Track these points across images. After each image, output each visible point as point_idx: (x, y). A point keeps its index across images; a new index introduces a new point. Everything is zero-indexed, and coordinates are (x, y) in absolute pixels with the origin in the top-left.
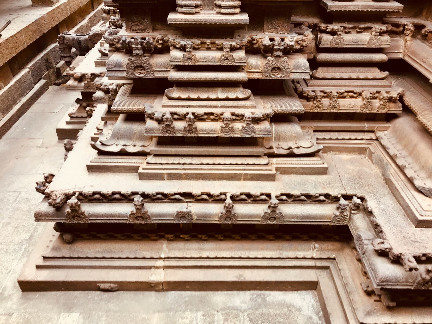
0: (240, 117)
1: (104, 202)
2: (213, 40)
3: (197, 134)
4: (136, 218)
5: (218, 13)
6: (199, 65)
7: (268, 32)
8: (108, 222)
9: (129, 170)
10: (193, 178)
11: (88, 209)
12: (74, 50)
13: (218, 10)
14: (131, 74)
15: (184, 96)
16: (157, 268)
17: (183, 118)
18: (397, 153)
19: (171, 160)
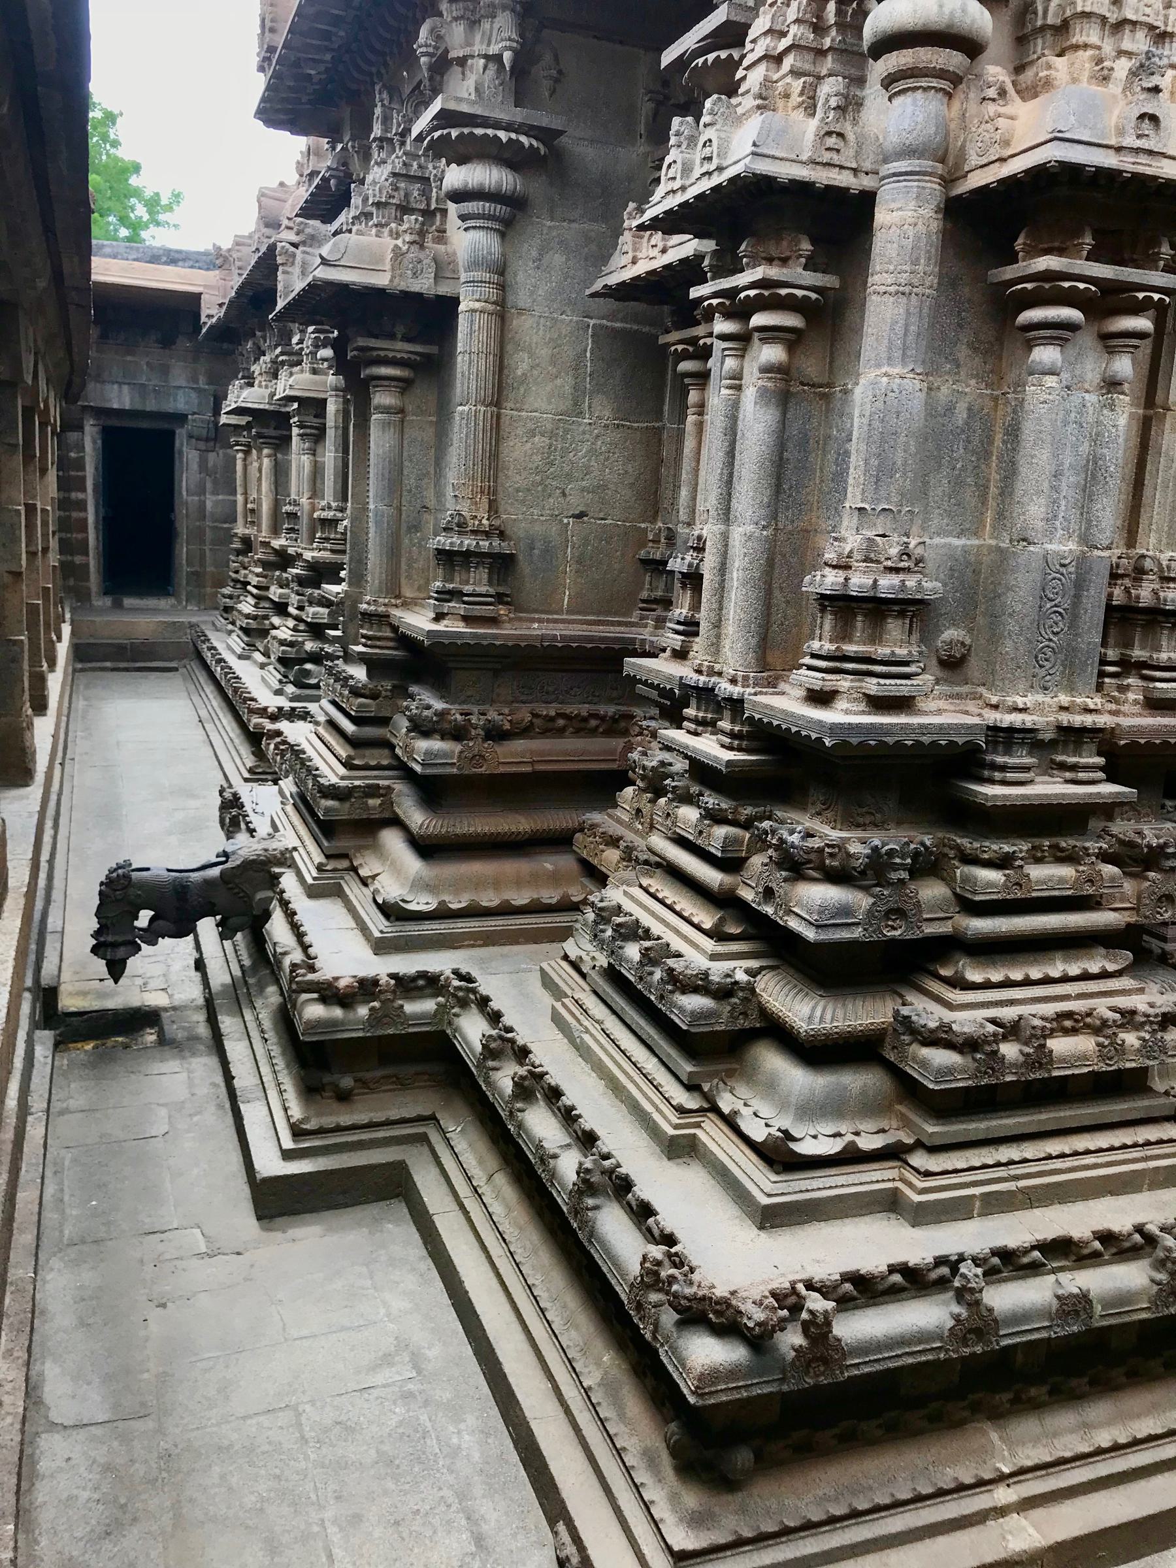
0: (1129, 1018)
1: (856, 1308)
2: (1055, 840)
3: (1049, 1071)
4: (965, 1342)
5: (1067, 781)
6: (1033, 898)
7: (1122, 820)
8: (891, 1365)
9: (868, 1204)
10: (1039, 1200)
11: (858, 1327)
12: (144, 918)
13: (1068, 775)
14: (874, 932)
15: (996, 976)
16: (1001, 1512)
17: (1012, 1030)
18: (537, 1282)
19: (976, 1157)
